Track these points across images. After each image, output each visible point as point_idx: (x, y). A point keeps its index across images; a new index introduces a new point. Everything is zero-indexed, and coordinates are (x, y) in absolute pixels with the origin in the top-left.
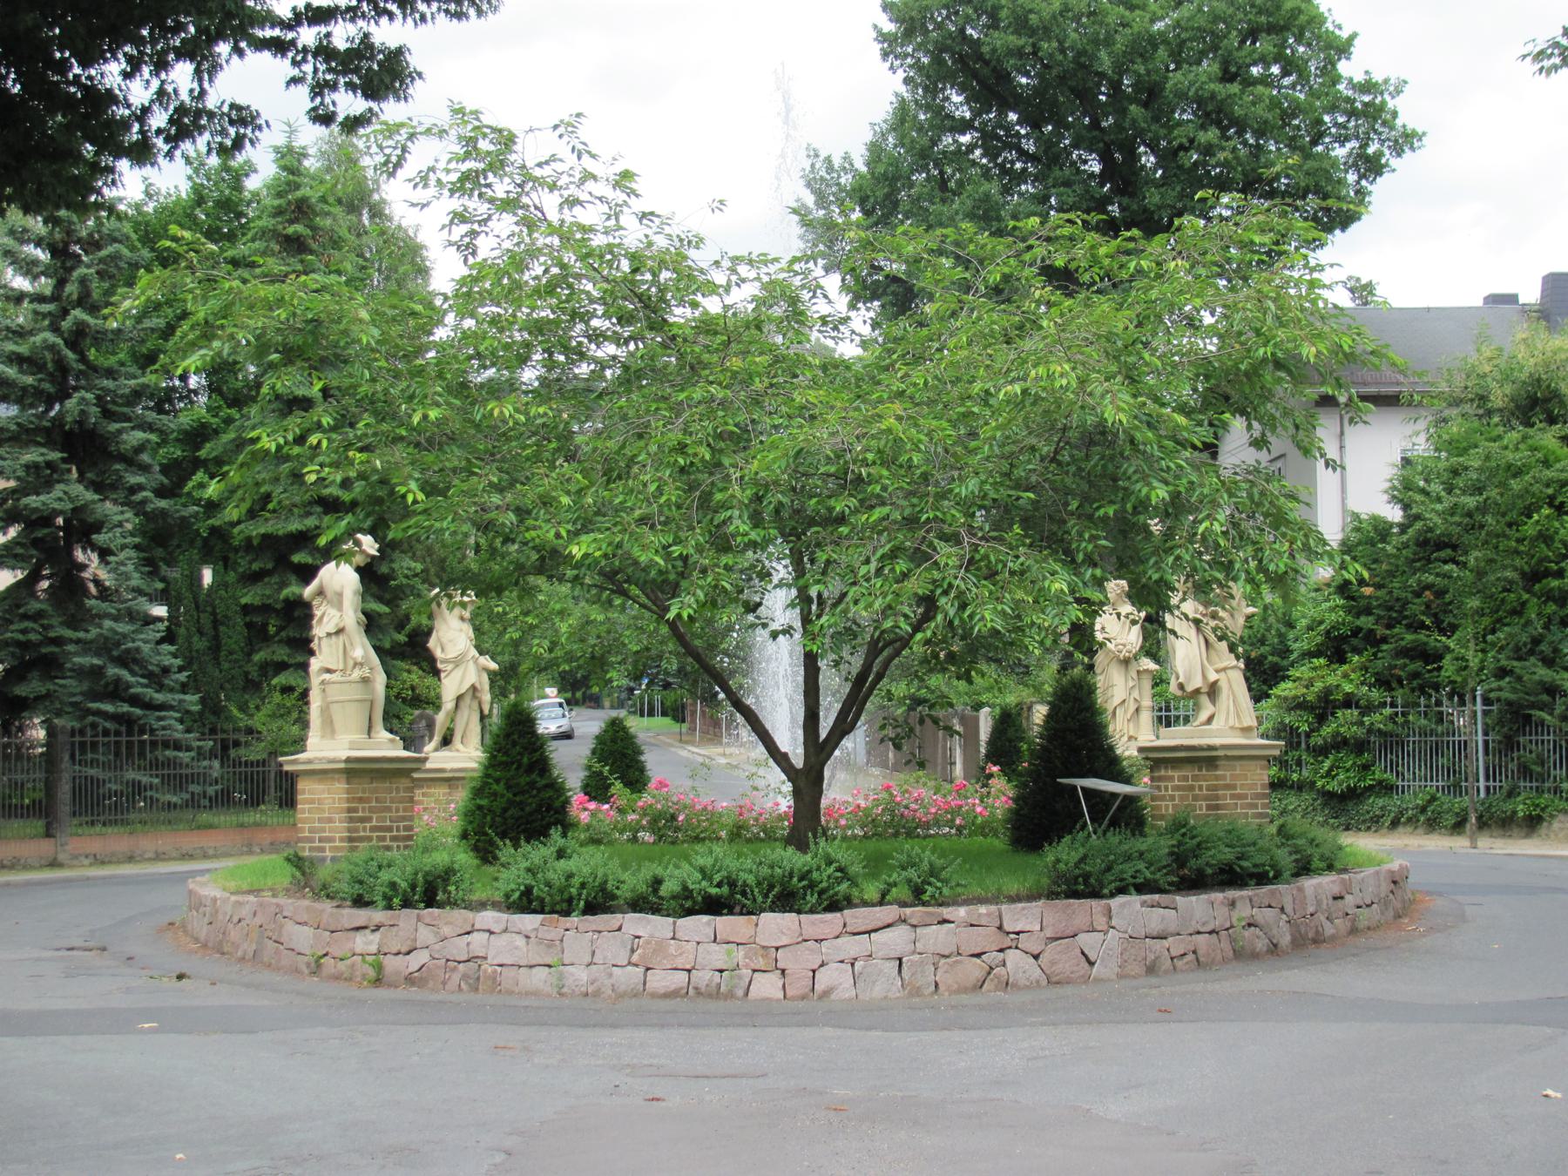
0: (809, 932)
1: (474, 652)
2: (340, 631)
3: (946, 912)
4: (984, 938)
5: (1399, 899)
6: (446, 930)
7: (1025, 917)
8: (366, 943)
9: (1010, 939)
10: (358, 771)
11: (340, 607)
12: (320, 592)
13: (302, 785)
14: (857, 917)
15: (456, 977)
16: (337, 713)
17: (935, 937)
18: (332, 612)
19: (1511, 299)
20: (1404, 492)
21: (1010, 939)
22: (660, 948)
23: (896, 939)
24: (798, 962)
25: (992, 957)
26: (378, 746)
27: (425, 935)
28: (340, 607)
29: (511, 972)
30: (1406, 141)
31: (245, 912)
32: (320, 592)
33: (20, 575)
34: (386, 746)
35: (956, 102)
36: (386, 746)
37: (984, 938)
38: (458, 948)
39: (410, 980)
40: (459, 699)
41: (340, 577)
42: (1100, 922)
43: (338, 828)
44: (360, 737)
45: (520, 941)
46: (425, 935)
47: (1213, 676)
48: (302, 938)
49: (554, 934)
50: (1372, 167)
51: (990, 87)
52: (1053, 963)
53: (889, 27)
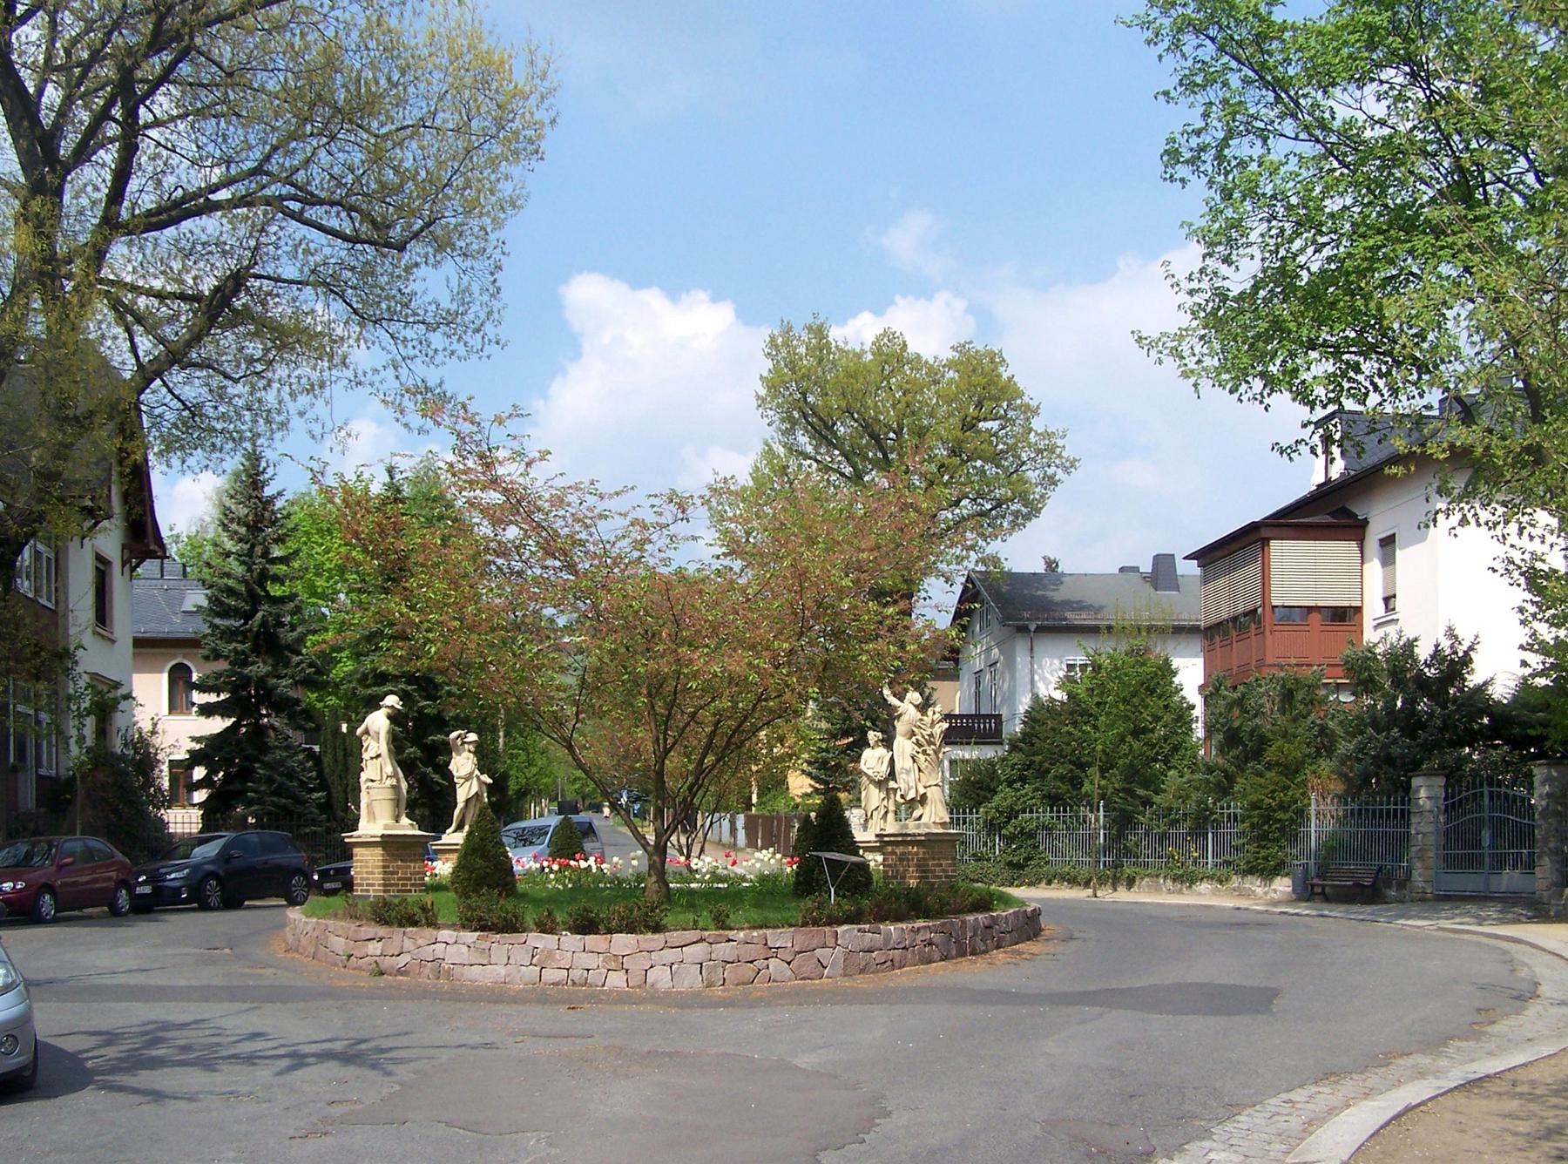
0: (644, 946)
1: (477, 772)
2: (379, 756)
3: (731, 934)
4: (755, 951)
5: (1029, 926)
6: (421, 942)
7: (781, 938)
8: (374, 948)
9: (771, 952)
10: (390, 844)
11: (378, 740)
12: (367, 732)
13: (356, 850)
14: (675, 937)
15: (427, 971)
16: (377, 807)
17: (724, 950)
18: (374, 744)
19: (1135, 569)
20: (1067, 682)
21: (771, 952)
22: (550, 954)
23: (698, 951)
24: (637, 964)
25: (760, 963)
26: (403, 827)
27: (408, 944)
28: (378, 740)
29: (459, 968)
30: (1070, 466)
31: (309, 928)
32: (367, 732)
33: (229, 722)
34: (407, 827)
35: (803, 440)
36: (407, 827)
37: (755, 951)
38: (427, 953)
39: (400, 972)
40: (468, 801)
41: (378, 721)
42: (831, 942)
43: (377, 878)
44: (391, 822)
45: (465, 949)
46: (408, 944)
47: (922, 791)
48: (339, 944)
49: (486, 945)
50: (1052, 481)
51: (823, 433)
52: (800, 967)
53: (763, 392)
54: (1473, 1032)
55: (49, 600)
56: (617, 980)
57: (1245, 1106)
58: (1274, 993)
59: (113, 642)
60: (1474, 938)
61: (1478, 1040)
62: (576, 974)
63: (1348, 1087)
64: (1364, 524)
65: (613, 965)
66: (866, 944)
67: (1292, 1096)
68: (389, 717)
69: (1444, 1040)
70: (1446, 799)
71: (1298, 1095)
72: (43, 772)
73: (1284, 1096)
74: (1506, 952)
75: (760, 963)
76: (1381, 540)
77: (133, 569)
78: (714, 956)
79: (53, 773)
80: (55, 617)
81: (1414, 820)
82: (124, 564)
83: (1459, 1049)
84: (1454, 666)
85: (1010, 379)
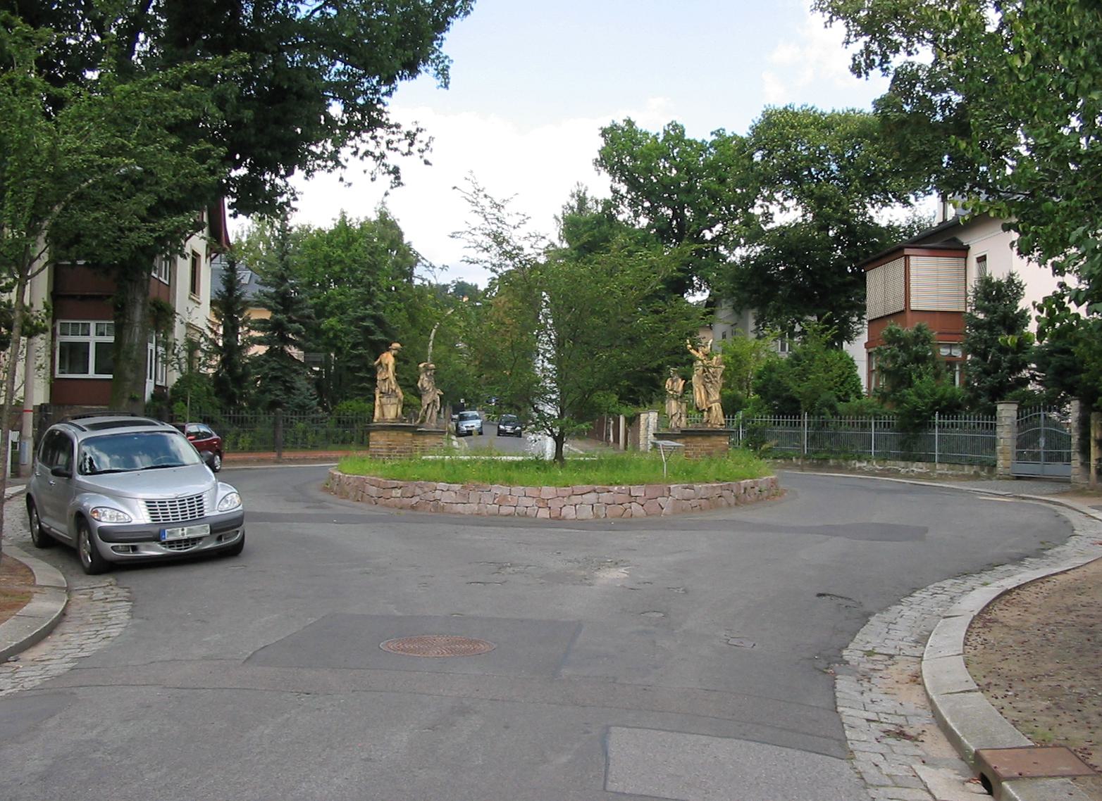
9: (632, 498)
12: (380, 363)
22: (505, 498)
23: (592, 497)
27: (418, 491)
38: (430, 496)
41: (388, 358)
42: (666, 493)
45: (453, 494)
54: (1039, 554)
55: (165, 279)
56: (544, 513)
57: (918, 589)
58: (926, 530)
59: (199, 303)
60: (1036, 503)
61: (1041, 558)
62: (520, 509)
63: (971, 582)
64: (967, 248)
65: (541, 505)
66: (686, 496)
67: (942, 584)
68: (394, 356)
69: (1022, 559)
70: (1018, 418)
71: (947, 583)
72: (158, 383)
73: (937, 584)
74: (1055, 511)
75: (627, 505)
76: (978, 258)
77: (211, 260)
78: (600, 500)
79: (163, 384)
80: (170, 288)
81: (998, 430)
82: (207, 257)
83: (1031, 563)
84: (476, 286)
85: (420, 71)
